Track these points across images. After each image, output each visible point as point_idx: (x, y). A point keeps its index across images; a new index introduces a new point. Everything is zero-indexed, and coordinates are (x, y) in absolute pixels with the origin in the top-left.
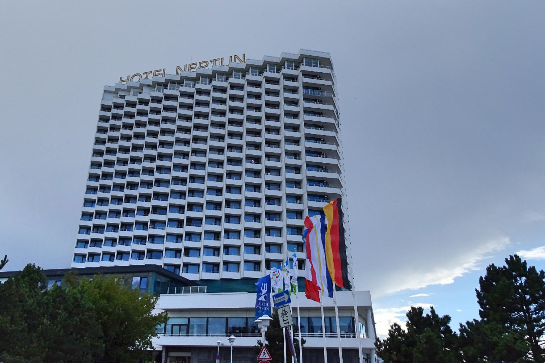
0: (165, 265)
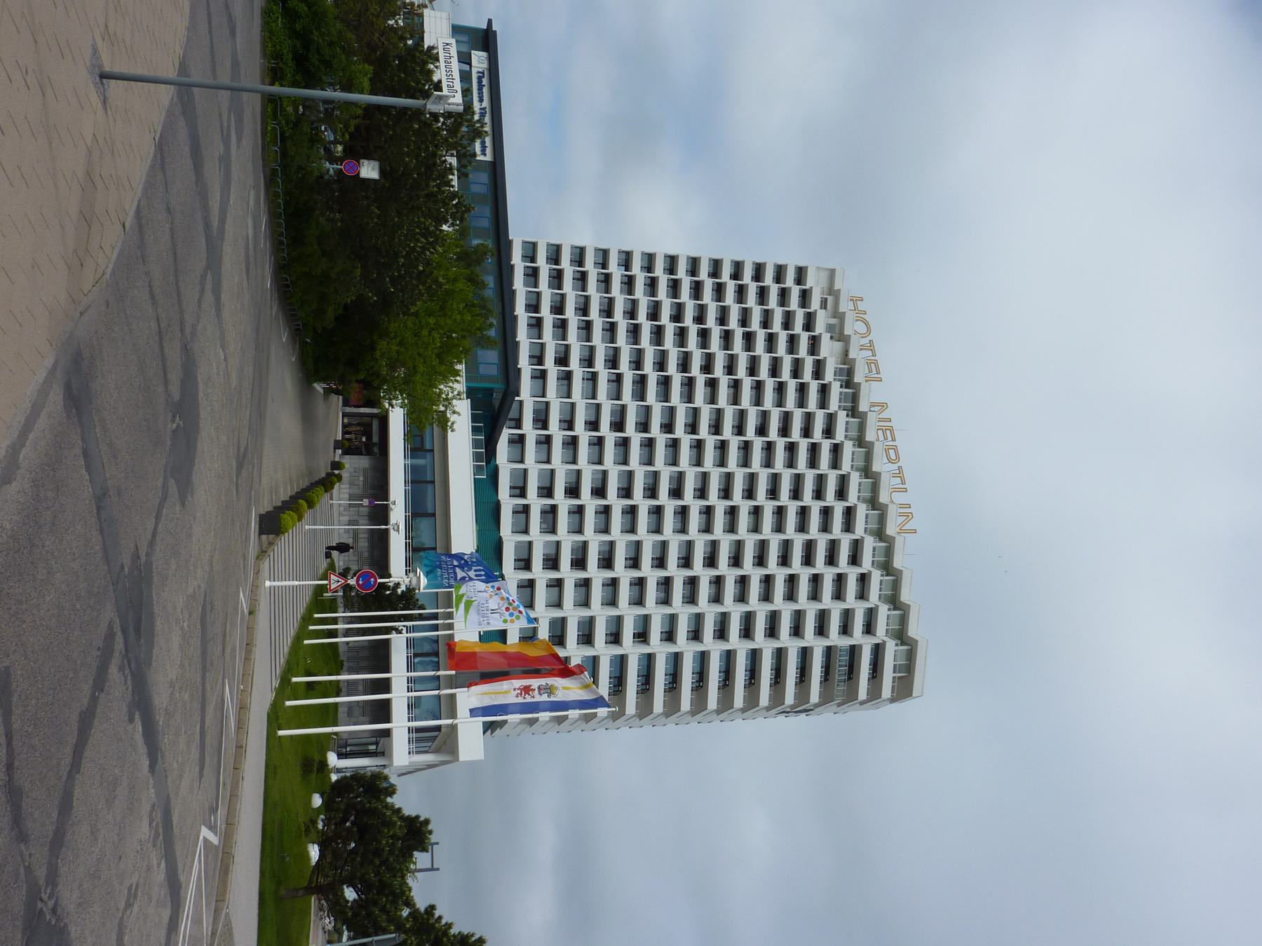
0: (521, 402)
